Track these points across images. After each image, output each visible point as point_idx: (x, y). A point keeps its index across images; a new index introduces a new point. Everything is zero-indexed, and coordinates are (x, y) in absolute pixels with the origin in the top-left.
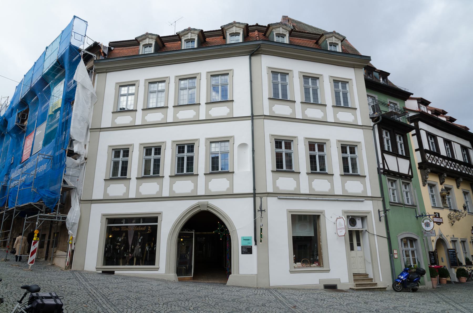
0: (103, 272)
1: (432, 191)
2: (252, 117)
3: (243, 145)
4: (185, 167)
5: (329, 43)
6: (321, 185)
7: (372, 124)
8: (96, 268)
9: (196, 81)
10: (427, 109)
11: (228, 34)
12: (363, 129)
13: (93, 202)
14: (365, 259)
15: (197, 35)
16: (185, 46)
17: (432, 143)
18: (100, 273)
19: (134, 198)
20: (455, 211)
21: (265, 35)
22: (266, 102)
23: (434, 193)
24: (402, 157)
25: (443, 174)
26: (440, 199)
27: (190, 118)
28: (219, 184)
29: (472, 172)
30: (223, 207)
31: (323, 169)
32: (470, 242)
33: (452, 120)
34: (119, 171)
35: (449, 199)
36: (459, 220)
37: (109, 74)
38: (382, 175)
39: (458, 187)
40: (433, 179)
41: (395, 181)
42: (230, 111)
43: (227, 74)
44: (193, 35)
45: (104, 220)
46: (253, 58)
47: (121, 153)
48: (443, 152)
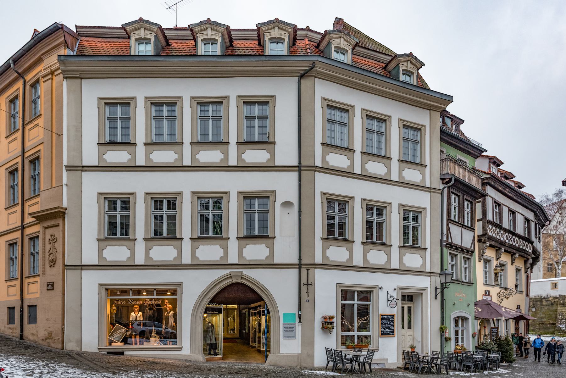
0: (108, 353)
1: (486, 267)
2: (300, 168)
3: (287, 204)
4: (211, 227)
5: (403, 70)
6: (377, 257)
7: (441, 187)
8: (99, 349)
9: (222, 108)
10: (498, 171)
11: (267, 39)
12: (430, 192)
13: (83, 268)
14: (414, 338)
16: (203, 51)
17: (496, 212)
18: (104, 354)
19: (144, 262)
20: (506, 289)
21: (318, 47)
22: (318, 244)
23: (487, 270)
24: (467, 227)
25: (500, 248)
26: (493, 275)
28: (256, 252)
30: (263, 279)
31: (380, 237)
33: (520, 186)
34: (117, 228)
35: (501, 276)
36: (507, 298)
38: (444, 248)
39: (512, 263)
40: (490, 254)
41: (456, 255)
42: (271, 156)
43: (267, 103)
44: (214, 33)
46: (303, 81)
48: (506, 225)
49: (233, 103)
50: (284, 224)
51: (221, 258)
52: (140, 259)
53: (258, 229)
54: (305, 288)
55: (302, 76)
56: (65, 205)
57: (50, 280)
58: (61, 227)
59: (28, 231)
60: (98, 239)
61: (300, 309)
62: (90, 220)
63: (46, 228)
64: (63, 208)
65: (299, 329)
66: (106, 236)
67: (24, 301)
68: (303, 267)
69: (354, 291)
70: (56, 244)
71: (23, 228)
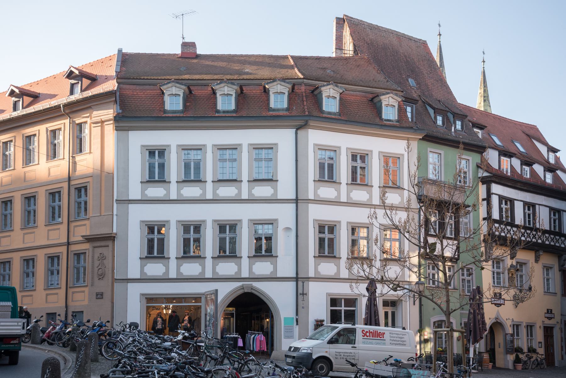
3: (288, 229)
15: (235, 91)
22: (311, 260)
27: (232, 197)
28: (263, 267)
29: (562, 244)
30: (268, 290)
32: (540, 327)
34: (155, 248)
37: (130, 132)
39: (537, 261)
45: (145, 301)
46: (299, 132)
47: (153, 229)
49: (245, 149)
50: (284, 246)
51: (236, 273)
52: (173, 274)
53: (264, 248)
54: (301, 295)
55: (298, 128)
56: (115, 231)
57: (99, 290)
58: (110, 248)
59: (73, 248)
60: (140, 258)
61: (297, 314)
62: (134, 243)
63: (95, 247)
64: (114, 234)
65: (296, 329)
66: (146, 255)
67: (69, 307)
68: (299, 280)
69: (342, 299)
70: (104, 261)
71: (68, 244)
